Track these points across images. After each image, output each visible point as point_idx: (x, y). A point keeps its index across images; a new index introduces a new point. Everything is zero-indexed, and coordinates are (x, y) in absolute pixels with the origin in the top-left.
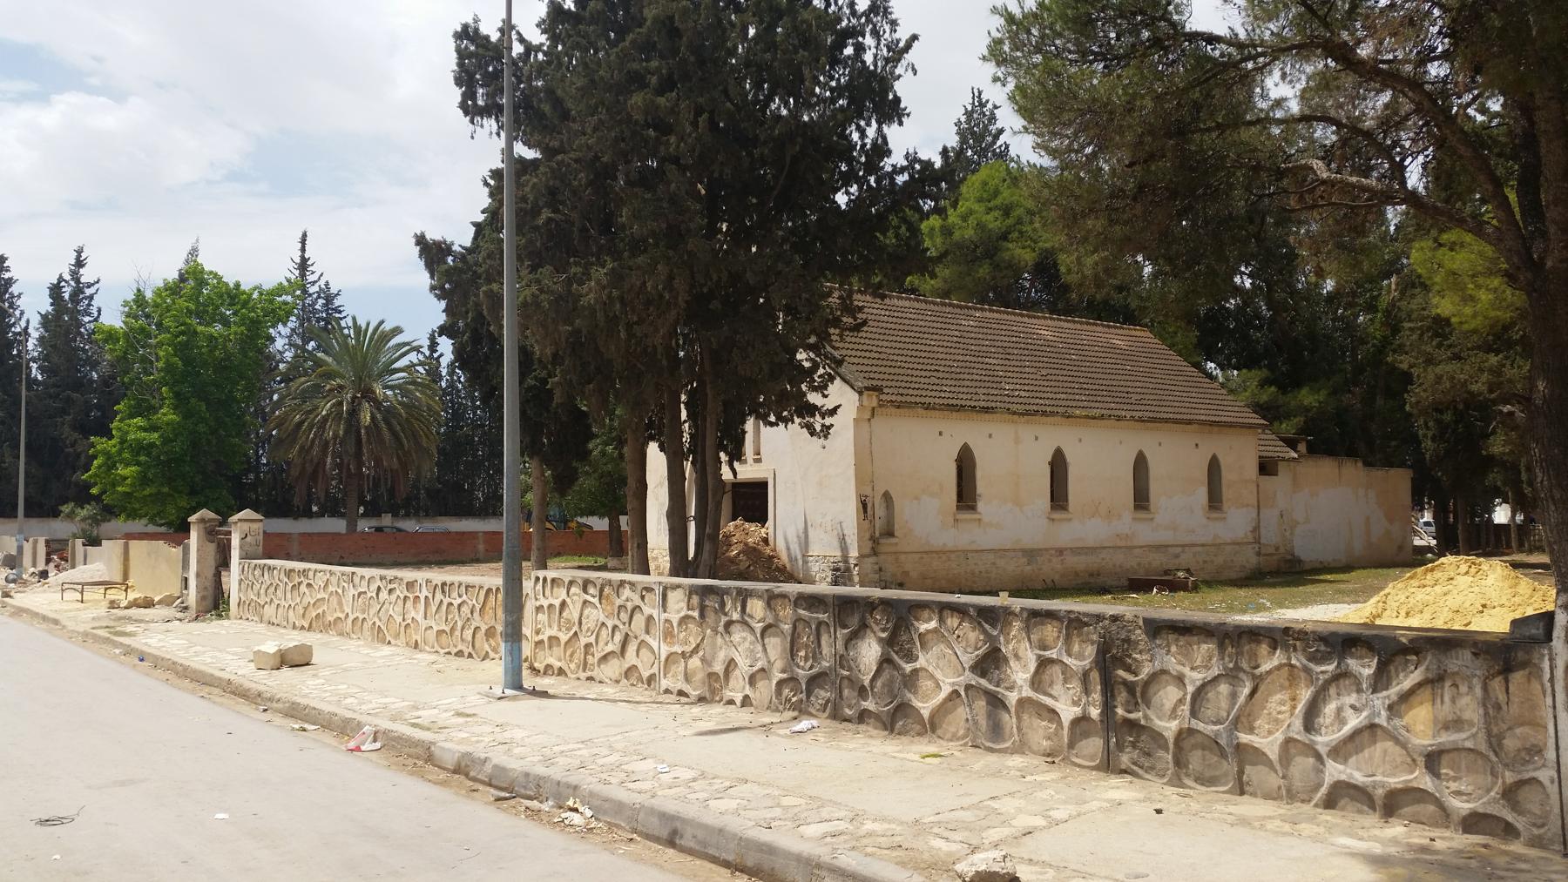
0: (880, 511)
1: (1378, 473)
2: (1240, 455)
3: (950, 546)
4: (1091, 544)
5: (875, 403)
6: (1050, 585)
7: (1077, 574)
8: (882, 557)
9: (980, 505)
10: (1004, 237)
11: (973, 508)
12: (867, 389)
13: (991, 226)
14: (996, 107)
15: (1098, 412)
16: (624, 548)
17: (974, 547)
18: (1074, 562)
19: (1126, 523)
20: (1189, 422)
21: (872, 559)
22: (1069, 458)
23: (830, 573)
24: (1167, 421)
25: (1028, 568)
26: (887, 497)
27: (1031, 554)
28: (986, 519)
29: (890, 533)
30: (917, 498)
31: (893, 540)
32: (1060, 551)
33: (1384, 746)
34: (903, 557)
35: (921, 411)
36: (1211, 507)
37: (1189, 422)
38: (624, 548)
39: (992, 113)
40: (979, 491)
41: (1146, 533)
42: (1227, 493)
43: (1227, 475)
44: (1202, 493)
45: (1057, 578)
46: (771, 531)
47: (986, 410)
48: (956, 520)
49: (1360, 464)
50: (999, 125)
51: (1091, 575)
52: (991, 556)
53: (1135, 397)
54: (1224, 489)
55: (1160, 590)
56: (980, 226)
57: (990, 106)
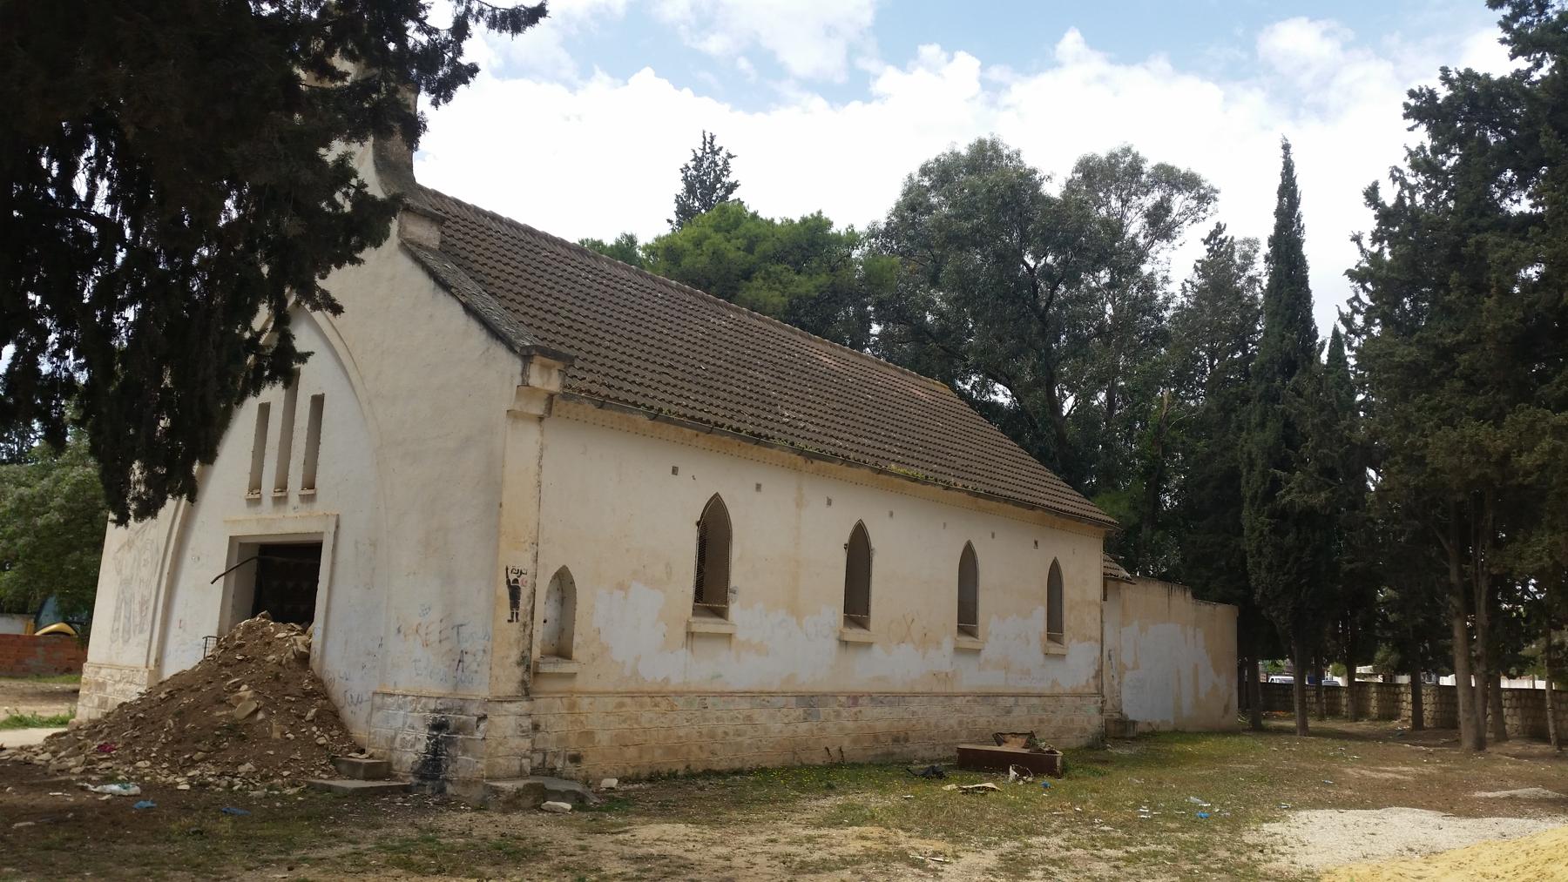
0: (545, 608)
1: (1206, 608)
2: (1085, 565)
3: (676, 682)
4: (898, 688)
5: (554, 385)
6: (837, 758)
7: (876, 737)
8: (540, 702)
9: (734, 609)
10: (747, 275)
11: (721, 613)
12: (544, 352)
13: (731, 255)
14: (730, 156)
15: (921, 474)
16: (1457, 743)
17: (717, 686)
18: (881, 718)
19: (942, 657)
20: (1032, 506)
21: (521, 706)
22: (875, 543)
23: (424, 734)
24: (1007, 500)
25: (804, 726)
26: (563, 583)
27: (809, 701)
28: (741, 636)
29: (562, 651)
30: (621, 586)
31: (566, 667)
32: (854, 699)
33: (510, 687)
34: (584, 703)
35: (642, 420)
36: (1050, 638)
37: (1032, 506)
38: (1457, 743)
39: (726, 163)
40: (734, 581)
41: (973, 677)
42: (1069, 619)
43: (1070, 593)
44: (1041, 612)
45: (846, 744)
46: (316, 640)
47: (757, 439)
48: (691, 635)
49: (1189, 594)
50: (731, 179)
51: (896, 740)
52: (744, 706)
53: (960, 461)
54: (1066, 613)
55: (1022, 773)
56: (717, 255)
57: (723, 154)
